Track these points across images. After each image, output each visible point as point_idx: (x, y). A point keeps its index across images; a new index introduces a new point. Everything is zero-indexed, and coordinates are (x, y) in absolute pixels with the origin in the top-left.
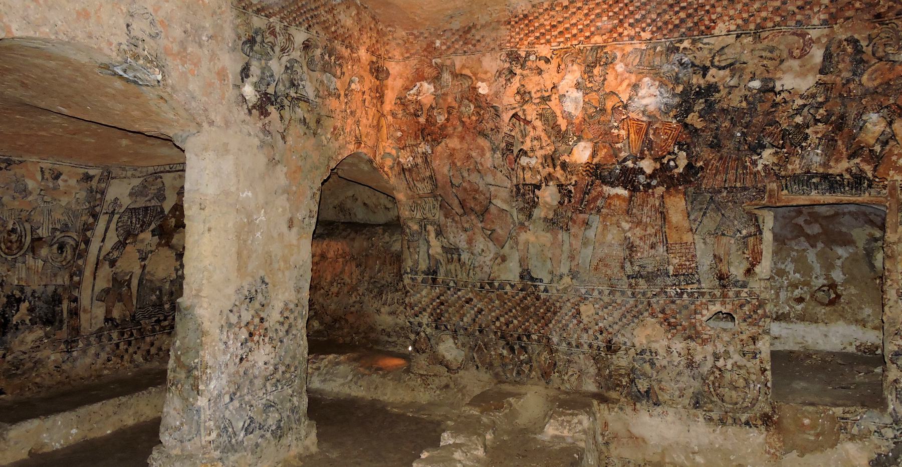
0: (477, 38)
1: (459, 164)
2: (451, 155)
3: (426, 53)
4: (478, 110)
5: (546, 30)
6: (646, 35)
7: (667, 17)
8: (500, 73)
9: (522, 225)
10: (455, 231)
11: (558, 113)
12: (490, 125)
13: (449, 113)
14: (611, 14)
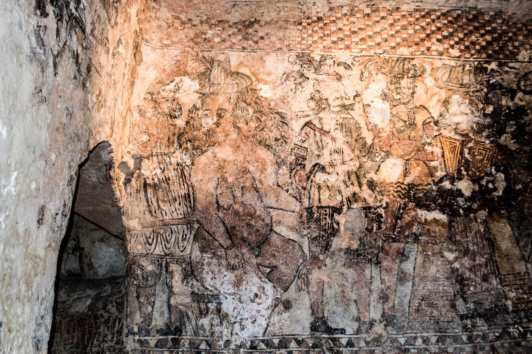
0: (261, 34)
1: (230, 180)
2: (221, 168)
3: (191, 44)
4: (259, 115)
5: (345, 36)
6: (455, 52)
7: (473, 38)
8: (287, 76)
9: (315, 258)
10: (216, 269)
11: (363, 124)
12: (275, 134)
13: (219, 116)
14: (417, 27)
